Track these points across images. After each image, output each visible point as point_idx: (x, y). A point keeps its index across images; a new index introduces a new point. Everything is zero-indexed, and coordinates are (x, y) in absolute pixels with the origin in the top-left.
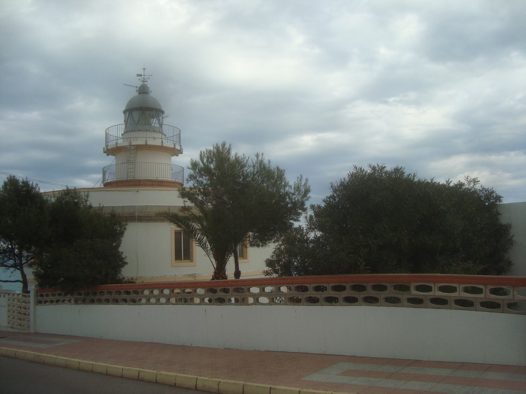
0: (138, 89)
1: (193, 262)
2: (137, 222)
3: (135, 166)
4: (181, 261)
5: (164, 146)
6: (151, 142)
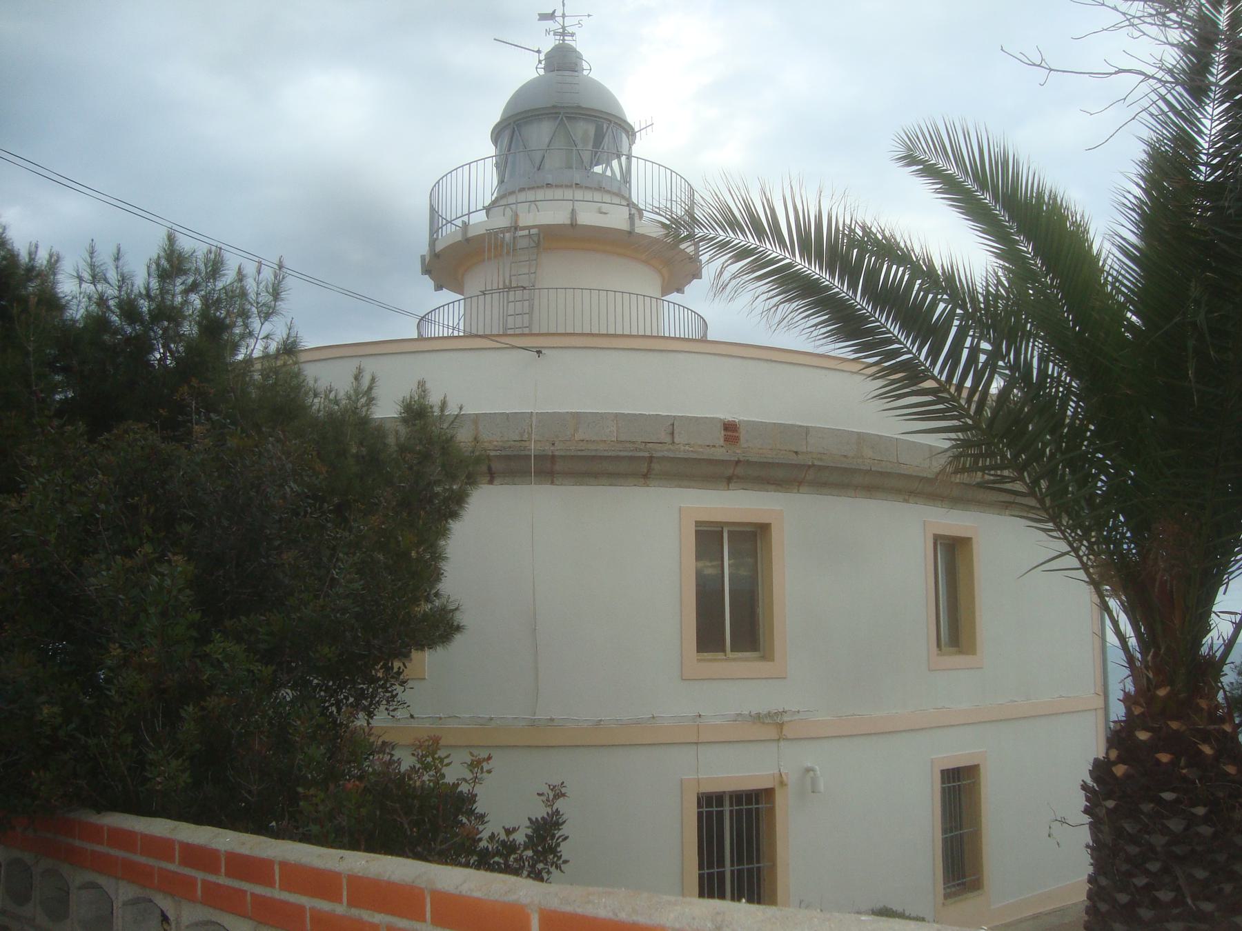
0: (542, 57)
3: (532, 307)
4: (720, 655)
6: (587, 217)
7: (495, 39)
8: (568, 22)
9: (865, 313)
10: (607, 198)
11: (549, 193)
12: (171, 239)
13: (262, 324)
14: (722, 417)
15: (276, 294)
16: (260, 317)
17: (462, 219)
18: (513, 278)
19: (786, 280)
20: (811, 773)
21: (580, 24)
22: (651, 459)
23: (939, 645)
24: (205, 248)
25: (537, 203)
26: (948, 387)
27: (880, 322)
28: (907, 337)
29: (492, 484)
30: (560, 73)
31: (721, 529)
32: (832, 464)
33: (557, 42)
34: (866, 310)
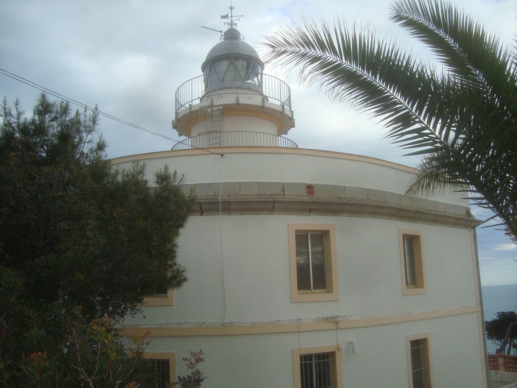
0: (223, 34)
1: (332, 292)
2: (222, 215)
3: (220, 140)
4: (309, 291)
5: (265, 106)
7: (202, 27)
8: (233, 19)
9: (382, 88)
10: (252, 92)
11: (227, 91)
12: (43, 96)
13: (87, 136)
14: (306, 182)
15: (94, 121)
16: (86, 132)
17: (189, 103)
18: (212, 128)
19: (338, 73)
20: (352, 344)
21: (239, 19)
22: (274, 202)
23: (407, 284)
24: (60, 100)
25: (221, 95)
26: (428, 126)
27: (390, 92)
28: (405, 100)
29: (202, 216)
30: (230, 40)
31: (307, 234)
32: (356, 203)
33: (229, 27)
34: (382, 86)
